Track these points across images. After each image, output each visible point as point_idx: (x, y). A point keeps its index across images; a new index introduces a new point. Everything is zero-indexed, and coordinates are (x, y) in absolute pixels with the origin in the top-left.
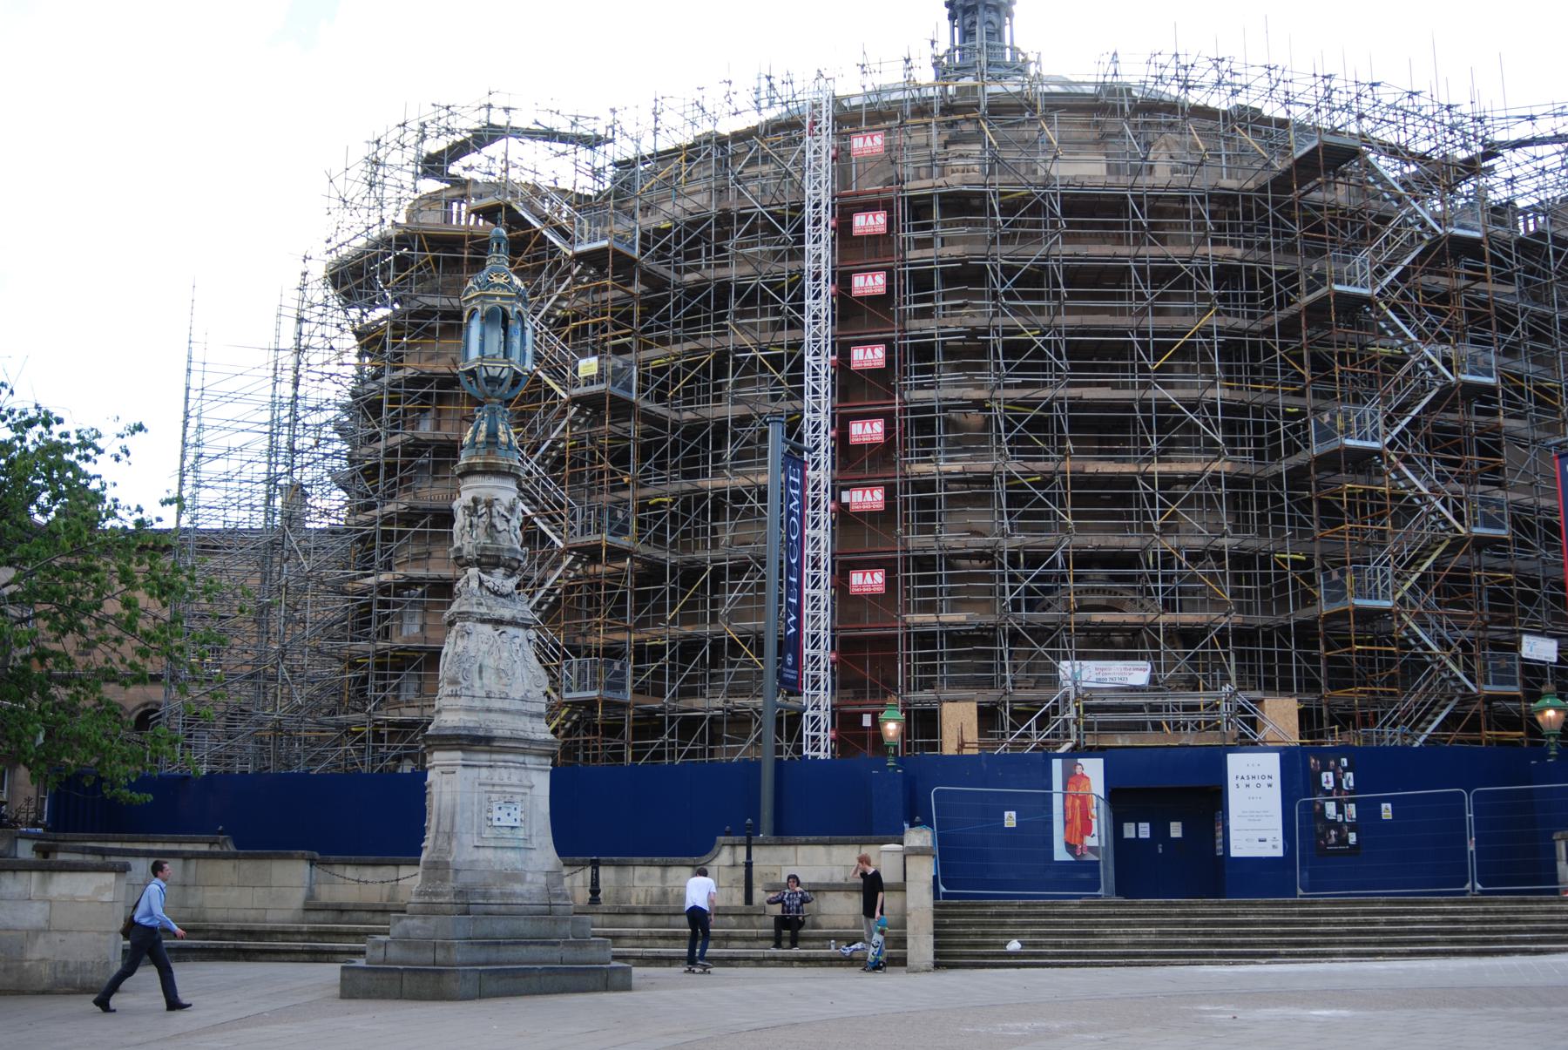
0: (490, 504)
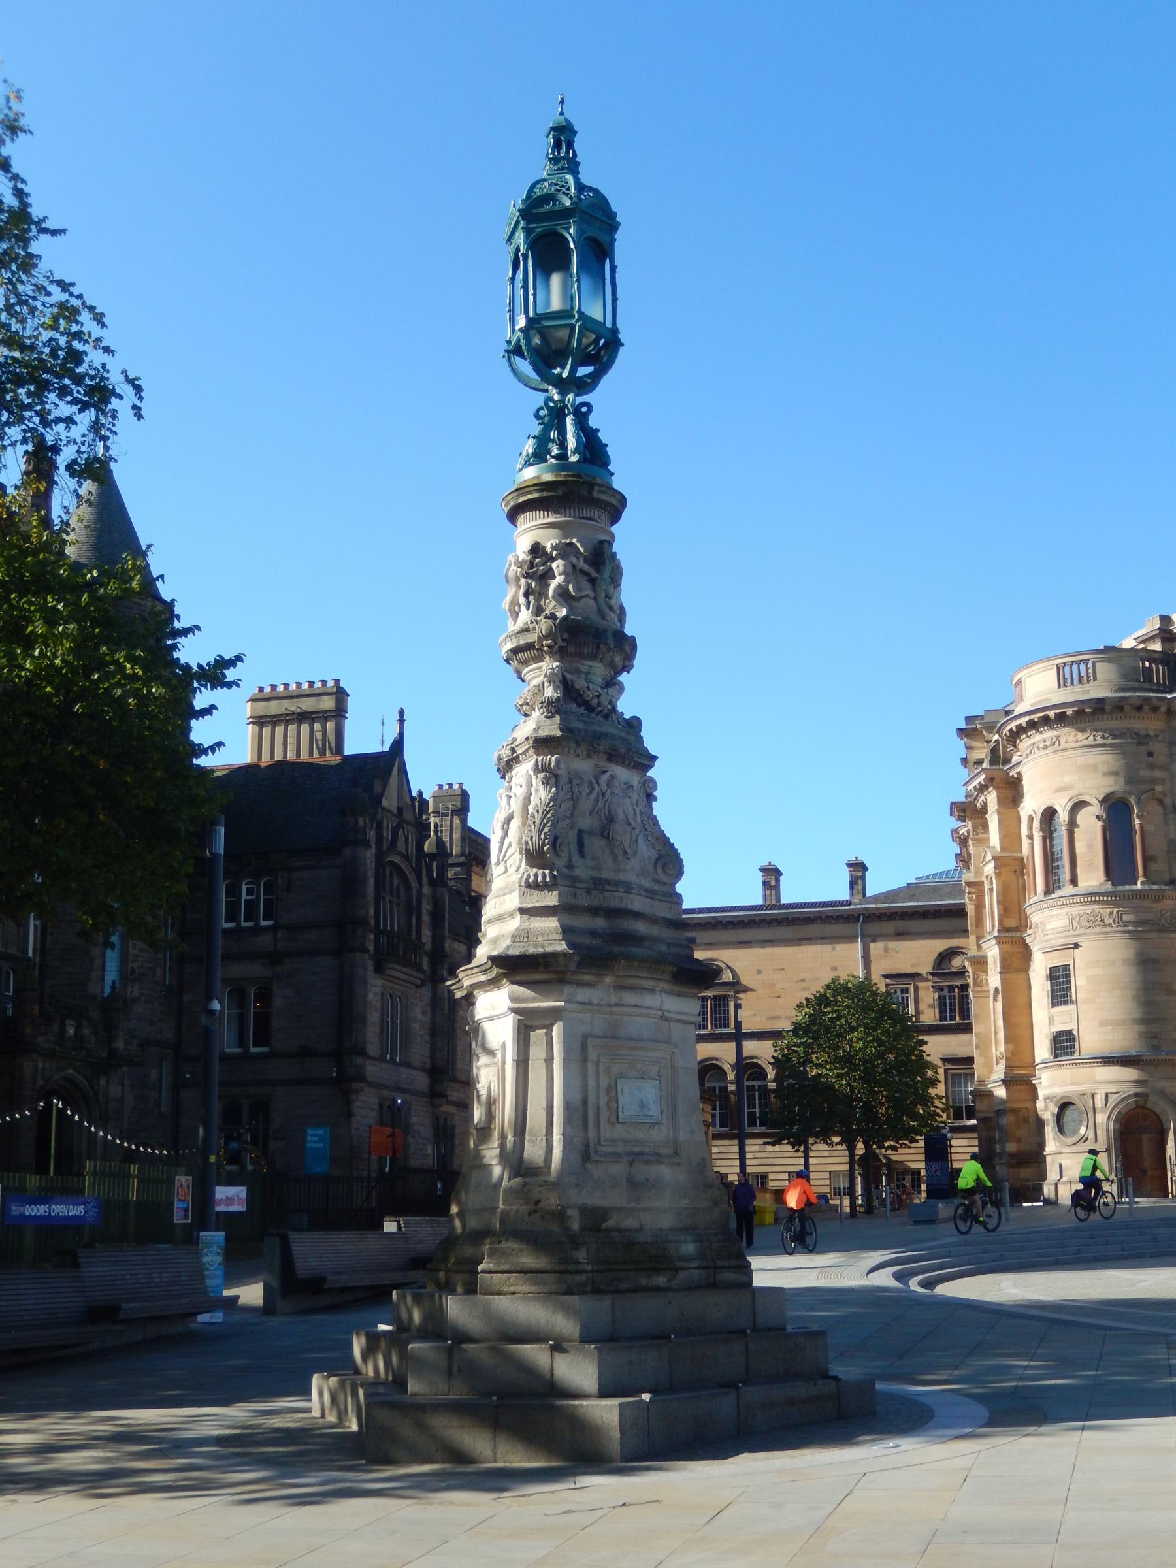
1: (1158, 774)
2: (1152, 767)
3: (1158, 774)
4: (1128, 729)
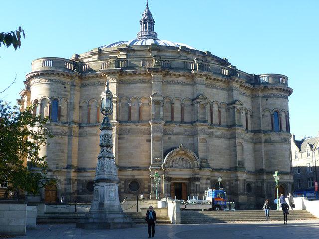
0: (107, 135)
2: (65, 91)
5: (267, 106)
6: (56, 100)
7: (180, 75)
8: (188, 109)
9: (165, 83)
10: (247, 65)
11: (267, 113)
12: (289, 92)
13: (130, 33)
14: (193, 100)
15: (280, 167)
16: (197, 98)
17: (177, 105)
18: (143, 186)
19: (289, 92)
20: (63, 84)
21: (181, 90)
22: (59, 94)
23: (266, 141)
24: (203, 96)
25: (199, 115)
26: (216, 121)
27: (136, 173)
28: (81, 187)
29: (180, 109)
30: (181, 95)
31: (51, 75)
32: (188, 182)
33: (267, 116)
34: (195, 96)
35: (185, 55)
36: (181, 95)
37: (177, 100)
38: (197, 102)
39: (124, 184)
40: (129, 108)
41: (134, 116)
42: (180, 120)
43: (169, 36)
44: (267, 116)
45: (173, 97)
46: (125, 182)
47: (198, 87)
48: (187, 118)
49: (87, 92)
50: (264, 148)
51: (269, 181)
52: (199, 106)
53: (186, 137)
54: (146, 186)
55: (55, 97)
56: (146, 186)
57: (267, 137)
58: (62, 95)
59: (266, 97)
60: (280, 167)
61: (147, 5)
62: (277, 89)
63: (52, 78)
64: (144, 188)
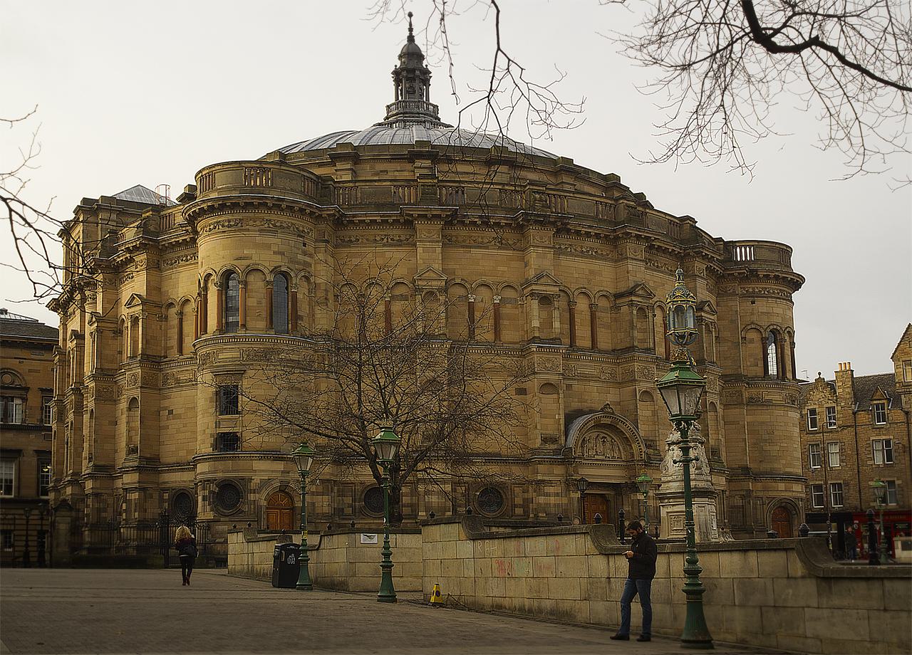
1: (308, 259)
3: (308, 259)
4: (292, 224)
5: (754, 318)
6: (285, 275)
7: (588, 234)
8: (604, 317)
9: (559, 252)
10: (720, 223)
11: (753, 335)
12: (796, 283)
13: (354, 105)
14: (618, 296)
15: (784, 462)
16: (631, 292)
17: (582, 305)
18: (513, 500)
19: (796, 283)
20: (299, 236)
21: (591, 272)
22: (292, 261)
23: (752, 402)
24: (643, 288)
25: (636, 333)
26: (583, 340)
27: (493, 469)
28: (349, 500)
29: (589, 318)
30: (589, 281)
31: (270, 208)
32: (613, 493)
33: (752, 341)
34: (623, 288)
35: (506, 171)
36: (589, 281)
37: (582, 296)
38: (631, 304)
39: (466, 495)
40: (471, 307)
41: (485, 334)
42: (588, 344)
43: (461, 107)
44: (752, 341)
45: (573, 287)
46: (468, 490)
47: (630, 268)
48: (605, 341)
49: (356, 261)
50: (747, 417)
51: (760, 494)
52: (635, 312)
53: (605, 385)
54: (518, 501)
55: (283, 269)
56: (518, 501)
57: (754, 391)
58: (298, 263)
59: (752, 297)
60: (784, 462)
61: (411, 30)
62: (777, 277)
63: (273, 217)
64: (516, 506)
